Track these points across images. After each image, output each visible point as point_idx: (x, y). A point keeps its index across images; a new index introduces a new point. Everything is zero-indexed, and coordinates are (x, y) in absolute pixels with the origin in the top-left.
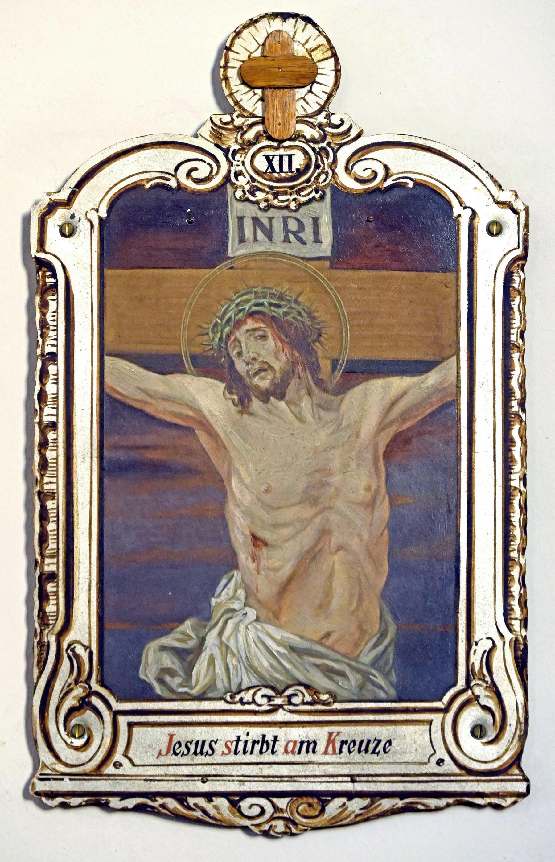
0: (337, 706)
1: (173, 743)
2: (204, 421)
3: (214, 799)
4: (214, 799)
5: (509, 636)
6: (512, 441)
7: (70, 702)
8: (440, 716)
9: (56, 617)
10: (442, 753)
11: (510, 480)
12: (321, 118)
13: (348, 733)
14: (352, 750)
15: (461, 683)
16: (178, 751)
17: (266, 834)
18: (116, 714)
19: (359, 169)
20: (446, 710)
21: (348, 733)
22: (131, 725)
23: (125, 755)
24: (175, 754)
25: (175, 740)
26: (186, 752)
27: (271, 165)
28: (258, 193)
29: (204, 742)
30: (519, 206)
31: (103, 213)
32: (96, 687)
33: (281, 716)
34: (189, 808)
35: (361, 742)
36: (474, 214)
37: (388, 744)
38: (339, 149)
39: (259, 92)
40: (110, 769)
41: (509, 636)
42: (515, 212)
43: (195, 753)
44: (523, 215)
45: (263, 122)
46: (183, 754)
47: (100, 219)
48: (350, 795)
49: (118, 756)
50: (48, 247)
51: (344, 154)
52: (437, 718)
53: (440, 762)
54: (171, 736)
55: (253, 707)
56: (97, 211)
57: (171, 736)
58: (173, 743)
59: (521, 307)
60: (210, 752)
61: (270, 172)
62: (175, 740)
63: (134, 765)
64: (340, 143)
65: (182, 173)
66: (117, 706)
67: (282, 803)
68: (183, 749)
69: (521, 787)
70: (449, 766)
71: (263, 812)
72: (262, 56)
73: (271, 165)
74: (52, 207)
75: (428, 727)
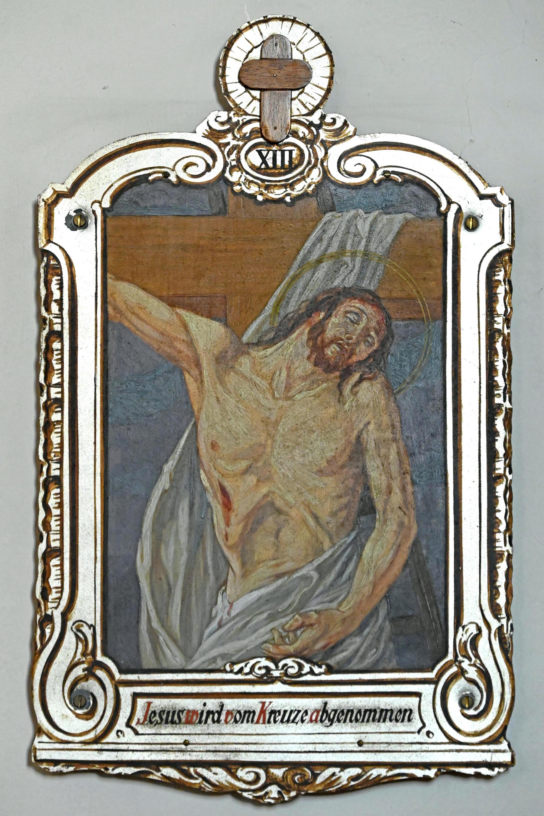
0: (323, 678)
1: (150, 712)
2: (510, 601)
3: (161, 768)
4: (161, 768)
5: (495, 624)
6: (497, 433)
7: (79, 671)
8: (433, 686)
9: (60, 590)
10: (431, 726)
11: (495, 469)
12: (315, 119)
13: (158, 704)
14: (341, 719)
15: (450, 657)
16: (153, 720)
17: (257, 802)
18: (117, 685)
19: (351, 165)
20: (435, 682)
21: (158, 704)
22: (136, 696)
23: (128, 725)
24: (151, 722)
25: (151, 709)
26: (159, 721)
27: (264, 161)
28: (252, 185)
29: (174, 712)
30: (503, 199)
31: (106, 204)
32: (100, 657)
33: (278, 687)
34: (190, 777)
35: (285, 712)
36: (459, 210)
37: (341, 714)
38: (330, 147)
39: (256, 94)
40: (112, 737)
41: (495, 624)
42: (498, 204)
43: (167, 722)
44: (508, 210)
45: (259, 121)
46: (157, 723)
47: (104, 210)
48: (344, 766)
49: (121, 724)
50: (56, 238)
51: (336, 152)
52: (427, 690)
53: (428, 733)
54: (149, 704)
55: (250, 677)
56: (100, 202)
57: (149, 704)
58: (150, 712)
59: (509, 310)
60: (177, 721)
61: (264, 169)
62: (151, 709)
63: (137, 733)
64: (333, 141)
65: (180, 167)
66: (118, 676)
67: (278, 772)
68: (157, 718)
69: (506, 758)
70: (439, 737)
71: (258, 777)
72: (261, 58)
73: (264, 161)
74: (59, 196)
75: (418, 699)
